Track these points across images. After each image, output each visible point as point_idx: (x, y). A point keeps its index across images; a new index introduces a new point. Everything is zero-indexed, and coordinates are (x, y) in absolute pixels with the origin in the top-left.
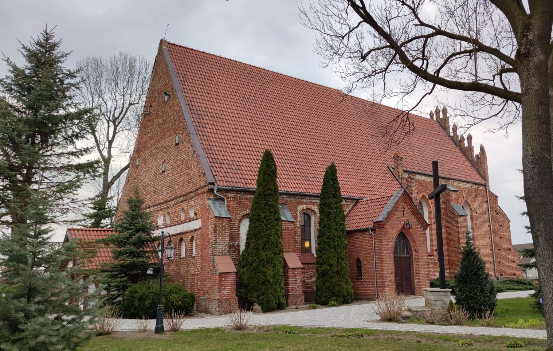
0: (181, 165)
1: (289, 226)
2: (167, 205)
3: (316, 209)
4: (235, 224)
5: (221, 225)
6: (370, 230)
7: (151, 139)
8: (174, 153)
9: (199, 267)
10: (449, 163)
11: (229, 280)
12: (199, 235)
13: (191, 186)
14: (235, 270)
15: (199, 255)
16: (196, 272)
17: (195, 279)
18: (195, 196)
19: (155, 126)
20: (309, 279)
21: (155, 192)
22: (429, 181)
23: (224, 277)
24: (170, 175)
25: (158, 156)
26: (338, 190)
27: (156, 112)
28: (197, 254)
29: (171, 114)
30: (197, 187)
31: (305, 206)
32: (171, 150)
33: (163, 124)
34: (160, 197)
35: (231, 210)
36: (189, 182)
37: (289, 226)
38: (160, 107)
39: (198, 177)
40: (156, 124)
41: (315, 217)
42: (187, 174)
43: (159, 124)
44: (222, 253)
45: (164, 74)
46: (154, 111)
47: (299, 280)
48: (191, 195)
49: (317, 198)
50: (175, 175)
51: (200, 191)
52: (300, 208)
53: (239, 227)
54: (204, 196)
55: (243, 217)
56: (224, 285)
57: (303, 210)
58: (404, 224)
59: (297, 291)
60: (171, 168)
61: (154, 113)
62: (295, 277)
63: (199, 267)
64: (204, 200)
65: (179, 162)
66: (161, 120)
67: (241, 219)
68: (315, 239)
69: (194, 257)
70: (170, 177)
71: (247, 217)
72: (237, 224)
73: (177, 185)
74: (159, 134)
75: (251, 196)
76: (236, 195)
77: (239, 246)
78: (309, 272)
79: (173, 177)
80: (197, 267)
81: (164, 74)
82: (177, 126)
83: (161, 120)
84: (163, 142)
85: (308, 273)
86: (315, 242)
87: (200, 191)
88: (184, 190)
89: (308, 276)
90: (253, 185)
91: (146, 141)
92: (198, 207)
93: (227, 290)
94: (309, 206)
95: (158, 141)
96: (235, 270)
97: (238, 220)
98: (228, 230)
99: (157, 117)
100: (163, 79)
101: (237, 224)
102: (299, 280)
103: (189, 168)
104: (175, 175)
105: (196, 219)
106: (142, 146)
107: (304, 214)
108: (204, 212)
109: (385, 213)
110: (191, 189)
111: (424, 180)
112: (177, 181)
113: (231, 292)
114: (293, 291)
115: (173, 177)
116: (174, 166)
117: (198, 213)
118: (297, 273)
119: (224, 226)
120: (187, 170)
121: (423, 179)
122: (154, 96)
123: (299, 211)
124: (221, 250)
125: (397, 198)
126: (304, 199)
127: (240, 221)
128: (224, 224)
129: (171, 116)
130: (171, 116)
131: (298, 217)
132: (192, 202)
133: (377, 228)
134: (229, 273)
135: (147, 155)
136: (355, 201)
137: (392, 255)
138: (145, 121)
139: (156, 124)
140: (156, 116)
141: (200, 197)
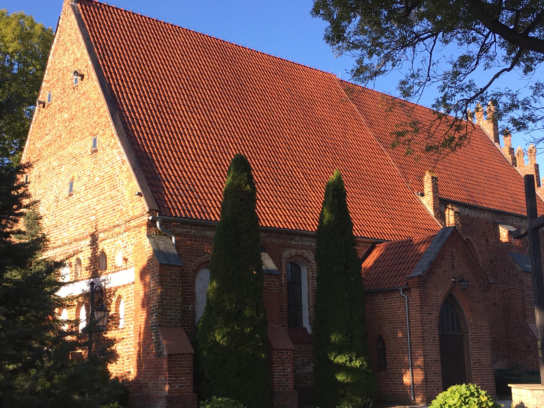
0: (102, 183)
1: (273, 281)
2: (76, 247)
3: (310, 256)
4: (187, 276)
5: (169, 278)
6: (401, 289)
7: (49, 145)
8: (89, 165)
9: (131, 344)
10: (503, 190)
11: (183, 367)
12: (131, 293)
13: (118, 216)
14: (193, 352)
15: (132, 326)
16: (126, 352)
17: (123, 364)
18: (125, 231)
19: (57, 124)
20: (300, 369)
21: (57, 226)
22: (476, 217)
23: (175, 361)
24: (82, 199)
25: (62, 170)
26: (349, 224)
27: (59, 102)
28: (127, 325)
29: (83, 105)
30: (128, 218)
31: (293, 252)
32: (84, 160)
33: (72, 118)
34: (65, 234)
35: (181, 255)
36: (114, 210)
37: (273, 281)
38: (65, 94)
39: (130, 202)
40: (58, 122)
41: (308, 269)
42: (112, 198)
43: (64, 121)
44: (171, 322)
45: (73, 44)
46: (56, 101)
47: (289, 370)
48: (117, 230)
49: (312, 239)
50: (91, 199)
51: (133, 223)
52: (286, 253)
53: (194, 282)
54: (140, 232)
55: (201, 266)
56: (175, 374)
57: (291, 257)
58: (454, 282)
59: (287, 386)
60: (84, 188)
61: (56, 104)
62: (283, 364)
63: (131, 344)
64: (141, 238)
65: (97, 179)
66: (66, 115)
67: (197, 269)
68: (309, 304)
69: (122, 329)
70: (82, 202)
71: (206, 267)
72: (191, 276)
73: (94, 215)
74: (63, 136)
75: (211, 234)
76: (189, 230)
77: (194, 313)
78: (300, 357)
79: (86, 203)
80: (127, 345)
81: (73, 44)
82: (95, 122)
83: (66, 115)
84: (70, 149)
85: (299, 359)
86: (309, 309)
87: (133, 223)
88: (106, 222)
89: (299, 363)
90: (215, 215)
91: (42, 148)
92: (131, 248)
93: (180, 383)
94: (300, 252)
95: (62, 148)
96: (193, 352)
97: (193, 270)
98: (179, 286)
99: (61, 110)
100: (71, 52)
101: (191, 276)
102: (289, 370)
103: (114, 187)
104: (91, 199)
105: (126, 269)
106: (35, 156)
107: (291, 263)
108: (140, 256)
109: (426, 263)
110: (118, 220)
111: (468, 215)
112: (94, 209)
113: (186, 386)
114: (281, 386)
115: (86, 203)
116: (90, 185)
117: (130, 259)
118: (286, 358)
119: (174, 280)
120: (111, 190)
121: (466, 213)
122: (56, 79)
123: (283, 259)
124: (168, 318)
125: (444, 240)
126: (292, 239)
127: (196, 272)
128: (173, 276)
129: (83, 109)
130: (83, 109)
131: (283, 269)
132: (120, 242)
133: (414, 288)
134: (183, 354)
135: (43, 169)
136: (370, 245)
137: (437, 332)
138: (40, 117)
139: (58, 122)
140: (59, 109)
141: (133, 233)
